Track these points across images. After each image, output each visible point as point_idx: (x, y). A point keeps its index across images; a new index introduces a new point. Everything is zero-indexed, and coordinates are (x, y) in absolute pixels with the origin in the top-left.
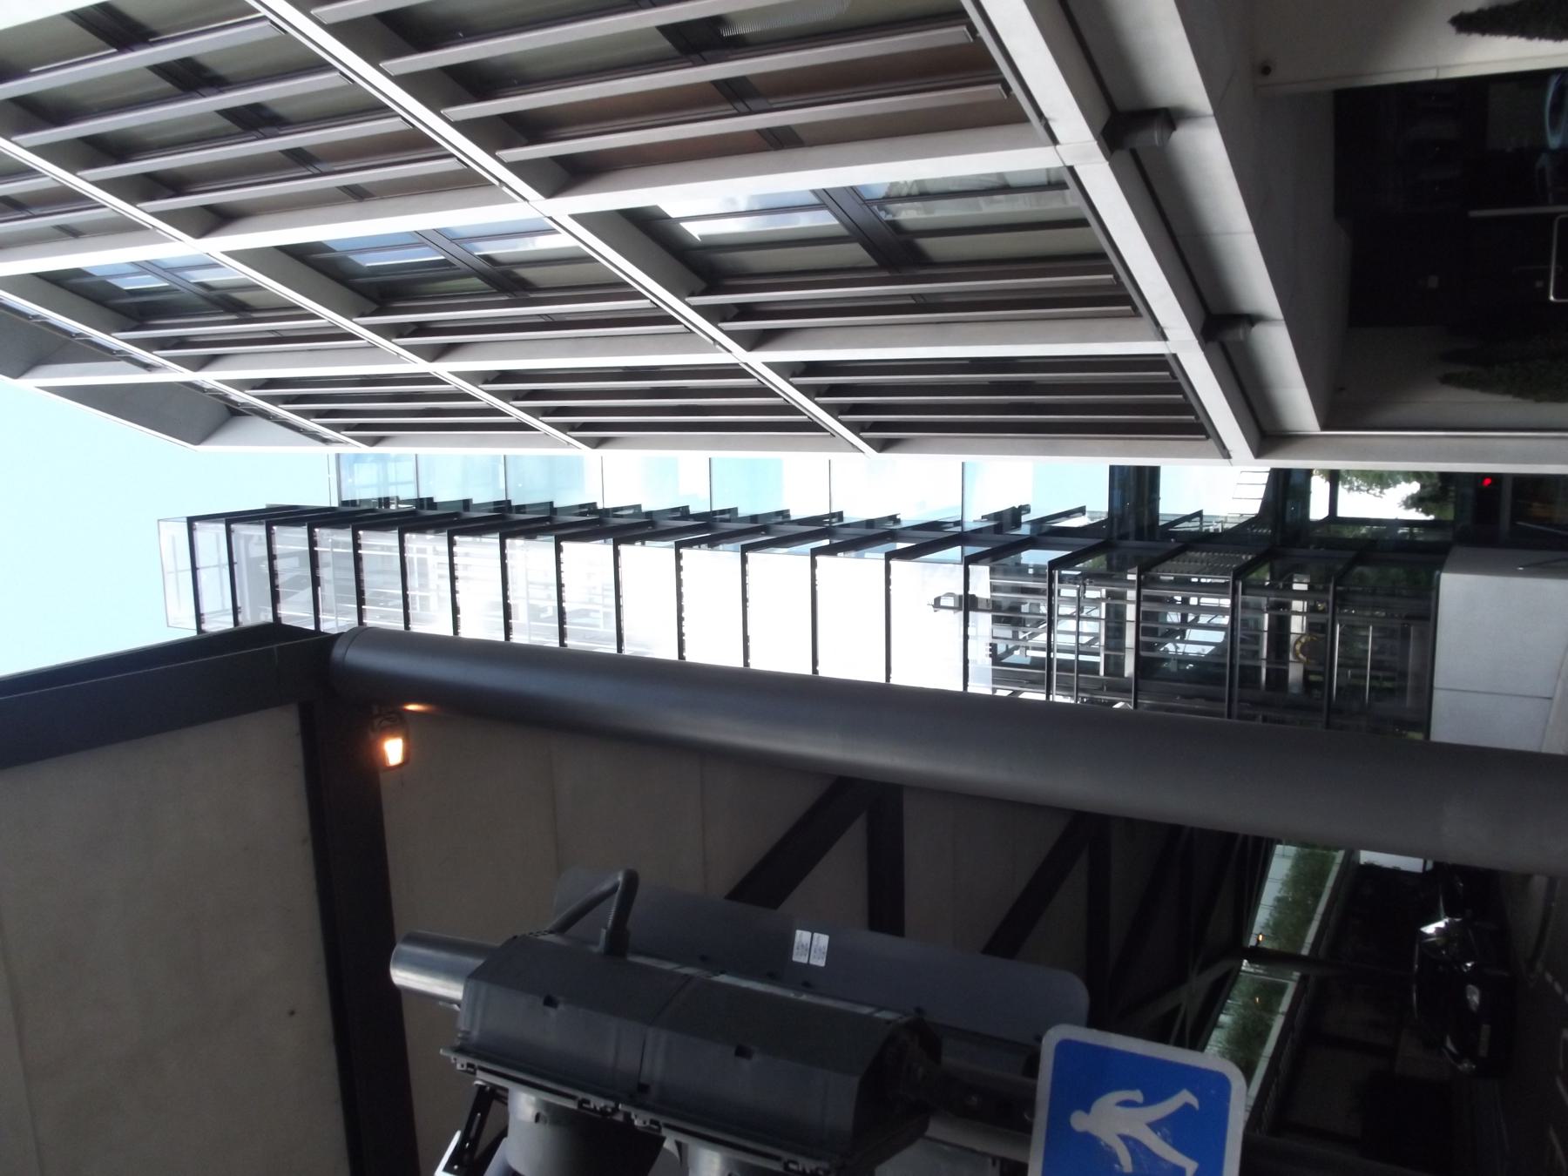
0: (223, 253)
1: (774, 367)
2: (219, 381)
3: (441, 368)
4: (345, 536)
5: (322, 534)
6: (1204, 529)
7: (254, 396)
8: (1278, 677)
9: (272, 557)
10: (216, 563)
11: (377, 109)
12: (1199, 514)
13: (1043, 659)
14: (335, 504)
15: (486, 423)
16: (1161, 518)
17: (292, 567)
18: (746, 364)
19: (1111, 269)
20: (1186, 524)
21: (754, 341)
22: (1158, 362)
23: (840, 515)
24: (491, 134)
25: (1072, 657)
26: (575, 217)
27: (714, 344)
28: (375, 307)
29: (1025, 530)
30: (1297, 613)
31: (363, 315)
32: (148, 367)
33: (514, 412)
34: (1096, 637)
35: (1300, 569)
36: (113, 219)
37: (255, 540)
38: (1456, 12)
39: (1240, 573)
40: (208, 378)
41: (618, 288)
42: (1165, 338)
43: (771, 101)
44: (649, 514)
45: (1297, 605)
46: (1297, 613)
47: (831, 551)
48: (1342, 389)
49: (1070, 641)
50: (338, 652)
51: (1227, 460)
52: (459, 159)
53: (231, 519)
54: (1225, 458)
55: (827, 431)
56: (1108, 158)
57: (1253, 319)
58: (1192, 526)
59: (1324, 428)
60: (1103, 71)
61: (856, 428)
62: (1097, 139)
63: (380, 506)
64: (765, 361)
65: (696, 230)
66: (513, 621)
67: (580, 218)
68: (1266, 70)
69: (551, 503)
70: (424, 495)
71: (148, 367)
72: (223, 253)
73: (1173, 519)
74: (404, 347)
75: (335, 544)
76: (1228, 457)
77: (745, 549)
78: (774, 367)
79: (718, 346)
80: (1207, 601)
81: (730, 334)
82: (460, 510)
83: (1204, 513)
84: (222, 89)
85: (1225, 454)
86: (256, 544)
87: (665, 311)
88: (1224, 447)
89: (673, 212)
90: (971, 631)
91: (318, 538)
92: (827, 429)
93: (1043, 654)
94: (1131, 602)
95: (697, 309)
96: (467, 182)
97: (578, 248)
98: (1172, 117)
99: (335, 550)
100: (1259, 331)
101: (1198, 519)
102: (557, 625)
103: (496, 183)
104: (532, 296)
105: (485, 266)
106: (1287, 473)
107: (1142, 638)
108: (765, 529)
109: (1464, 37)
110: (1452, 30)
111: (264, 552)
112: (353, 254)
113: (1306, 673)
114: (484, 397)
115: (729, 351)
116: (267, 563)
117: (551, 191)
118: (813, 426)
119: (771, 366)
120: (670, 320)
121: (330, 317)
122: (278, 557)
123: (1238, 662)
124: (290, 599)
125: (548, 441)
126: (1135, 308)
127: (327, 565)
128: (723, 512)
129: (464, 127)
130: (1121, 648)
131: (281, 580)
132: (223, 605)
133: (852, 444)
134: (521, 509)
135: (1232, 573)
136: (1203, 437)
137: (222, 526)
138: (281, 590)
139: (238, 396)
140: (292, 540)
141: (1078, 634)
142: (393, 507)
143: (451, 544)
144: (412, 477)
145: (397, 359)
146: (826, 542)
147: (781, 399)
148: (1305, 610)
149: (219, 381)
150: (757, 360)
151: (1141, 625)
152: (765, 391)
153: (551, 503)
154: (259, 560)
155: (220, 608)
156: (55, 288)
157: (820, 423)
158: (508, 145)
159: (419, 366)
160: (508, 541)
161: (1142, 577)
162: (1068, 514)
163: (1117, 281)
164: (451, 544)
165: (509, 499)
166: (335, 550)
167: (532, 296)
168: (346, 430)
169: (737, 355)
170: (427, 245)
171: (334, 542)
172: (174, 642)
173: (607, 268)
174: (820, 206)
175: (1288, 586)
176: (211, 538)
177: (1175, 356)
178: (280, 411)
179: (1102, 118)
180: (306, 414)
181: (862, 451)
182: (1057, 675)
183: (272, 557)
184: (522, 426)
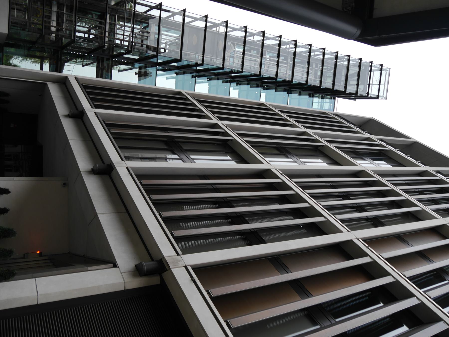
1: (210, 118)
3: (303, 129)
4: (336, 88)
5: (342, 89)
6: (82, 61)
8: (60, 6)
9: (358, 85)
10: (373, 85)
12: (83, 66)
13: (135, 25)
14: (337, 98)
15: (293, 113)
16: (96, 66)
17: (352, 82)
18: (218, 120)
19: (111, 133)
20: (88, 63)
21: (215, 126)
22: (97, 107)
23: (193, 77)
24: (283, 186)
25: (126, 24)
26: (263, 163)
27: (226, 126)
28: (319, 148)
29: (137, 65)
30: (54, 27)
31: (323, 146)
32: (382, 140)
33: (284, 116)
34: (119, 29)
35: (53, 42)
38: (9, 195)
39: (73, 41)
40: (367, 135)
41: (254, 145)
42: (95, 113)
43: (206, 187)
44: (248, 84)
45: (54, 29)
46: (54, 27)
47: (197, 65)
48: (40, 95)
49: (126, 29)
50: (359, 32)
51: (76, 77)
52: (292, 181)
53: (366, 97)
54: (77, 78)
55: (196, 99)
56: (112, 162)
57: (68, 116)
58: (86, 62)
59: (46, 84)
60: (113, 185)
61: (187, 99)
62: (115, 167)
63: (324, 97)
65: (229, 158)
66: (293, 56)
67: (262, 163)
68: (65, 184)
69: (276, 91)
70: (311, 98)
71: (382, 140)
73: (91, 65)
75: (339, 86)
76: (75, 78)
77: (223, 68)
78: (210, 118)
79: (226, 126)
80: (82, 35)
81: (222, 129)
82: (302, 92)
83: (82, 66)
85: (76, 79)
86: (361, 89)
88: (77, 81)
89: (234, 163)
90: (157, 36)
91: (344, 88)
92: (196, 100)
93: (135, 26)
94: (107, 37)
95: (231, 136)
96: (291, 175)
98: (93, 172)
99: (340, 84)
100: (67, 113)
101: (84, 64)
102: (280, 53)
103: (283, 174)
104: (276, 146)
105: (289, 156)
106: (56, 71)
107: (104, 26)
108: (215, 74)
109: (7, 188)
110: (10, 190)
111: (360, 87)
112: (322, 162)
113: (51, 8)
114: (292, 121)
115: (222, 124)
116: (359, 83)
117: (268, 171)
118: (200, 101)
119: (211, 119)
120: (240, 135)
121: (332, 146)
123: (74, 14)
124: (355, 72)
125: (276, 107)
126: (104, 122)
127: (343, 81)
128: (227, 82)
129: (290, 189)
130: (110, 24)
131: (356, 78)
132: (373, 73)
133: (189, 95)
134: (285, 90)
135: (75, 42)
136: (83, 85)
137: (372, 93)
138: (357, 75)
139: (359, 130)
140: (351, 89)
141: (124, 30)
142: (321, 95)
143: (307, 81)
144: (314, 104)
145: (315, 134)
146: (198, 68)
147: (208, 109)
148: (51, 27)
150: (215, 121)
151: (103, 35)
152: (214, 113)
153: (276, 91)
154: (361, 85)
155: (374, 72)
156: (402, 163)
157: (197, 102)
158: (279, 183)
159: (309, 131)
160: (290, 80)
161: (103, 44)
162: (124, 70)
163: (109, 130)
164: (307, 81)
165: (288, 94)
166: (340, 84)
169: (220, 123)
170: (303, 162)
171: (339, 87)
172: (403, 43)
173: (254, 149)
174: (193, 159)
175: (57, 36)
176: (374, 92)
177: (92, 108)
178: (348, 124)
179: (113, 173)
180: (341, 123)
181: (186, 93)
182: (131, 17)
183: (358, 85)
184: (283, 112)
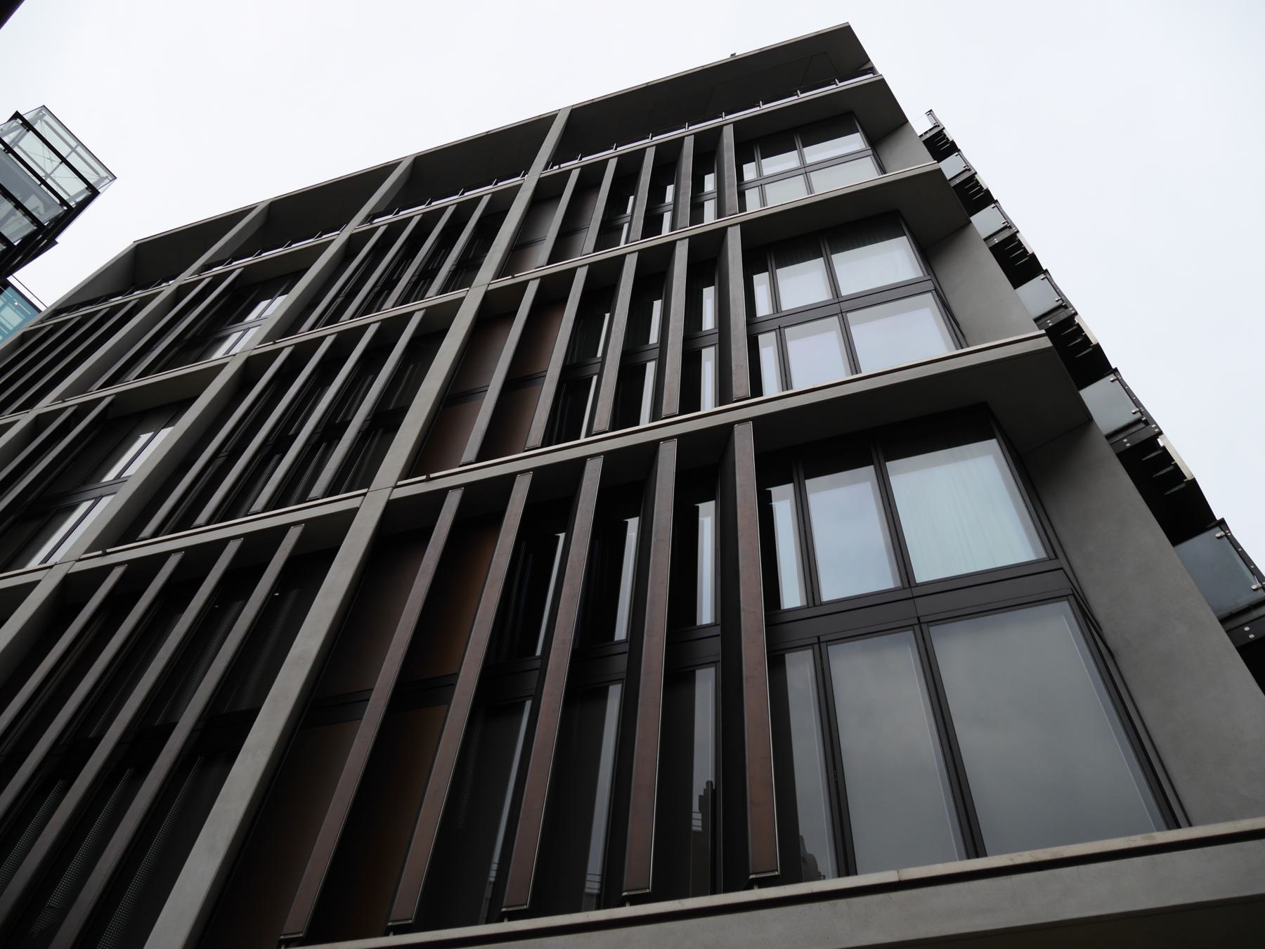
0: (19, 420)
2: (161, 292)
7: (73, 318)
9: (19, 205)
11: (279, 500)
15: (272, 336)
24: (142, 571)
32: (207, 267)
36: (126, 377)
37: (42, 210)
64: (41, 582)
72: (19, 420)
74: (66, 408)
84: (361, 433)
86: (38, 207)
87: (163, 535)
97: (23, 566)
121: (131, 383)
122: (15, 209)
139: (139, 294)
145: (62, 398)
149: (161, 292)
167: (11, 518)
168: (79, 320)
176: (72, 188)
178: (104, 307)
183: (19, 205)
